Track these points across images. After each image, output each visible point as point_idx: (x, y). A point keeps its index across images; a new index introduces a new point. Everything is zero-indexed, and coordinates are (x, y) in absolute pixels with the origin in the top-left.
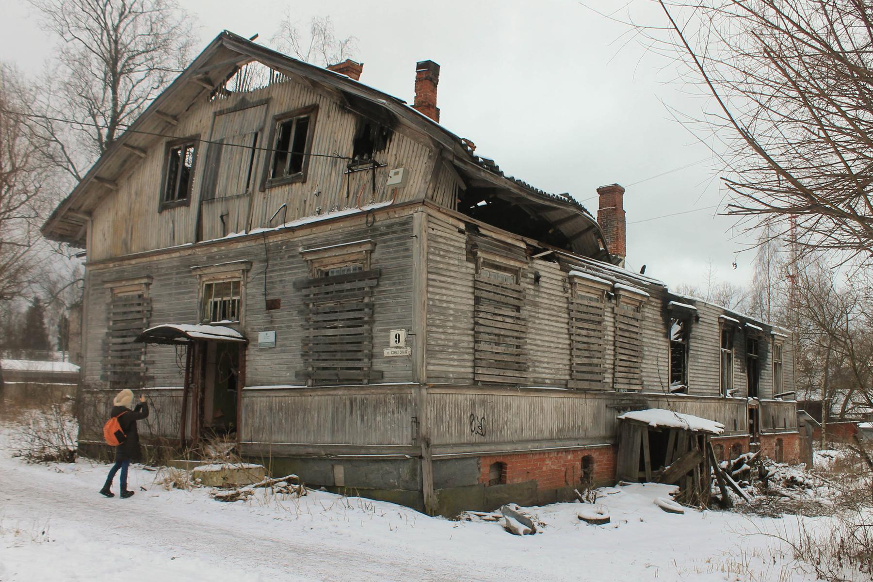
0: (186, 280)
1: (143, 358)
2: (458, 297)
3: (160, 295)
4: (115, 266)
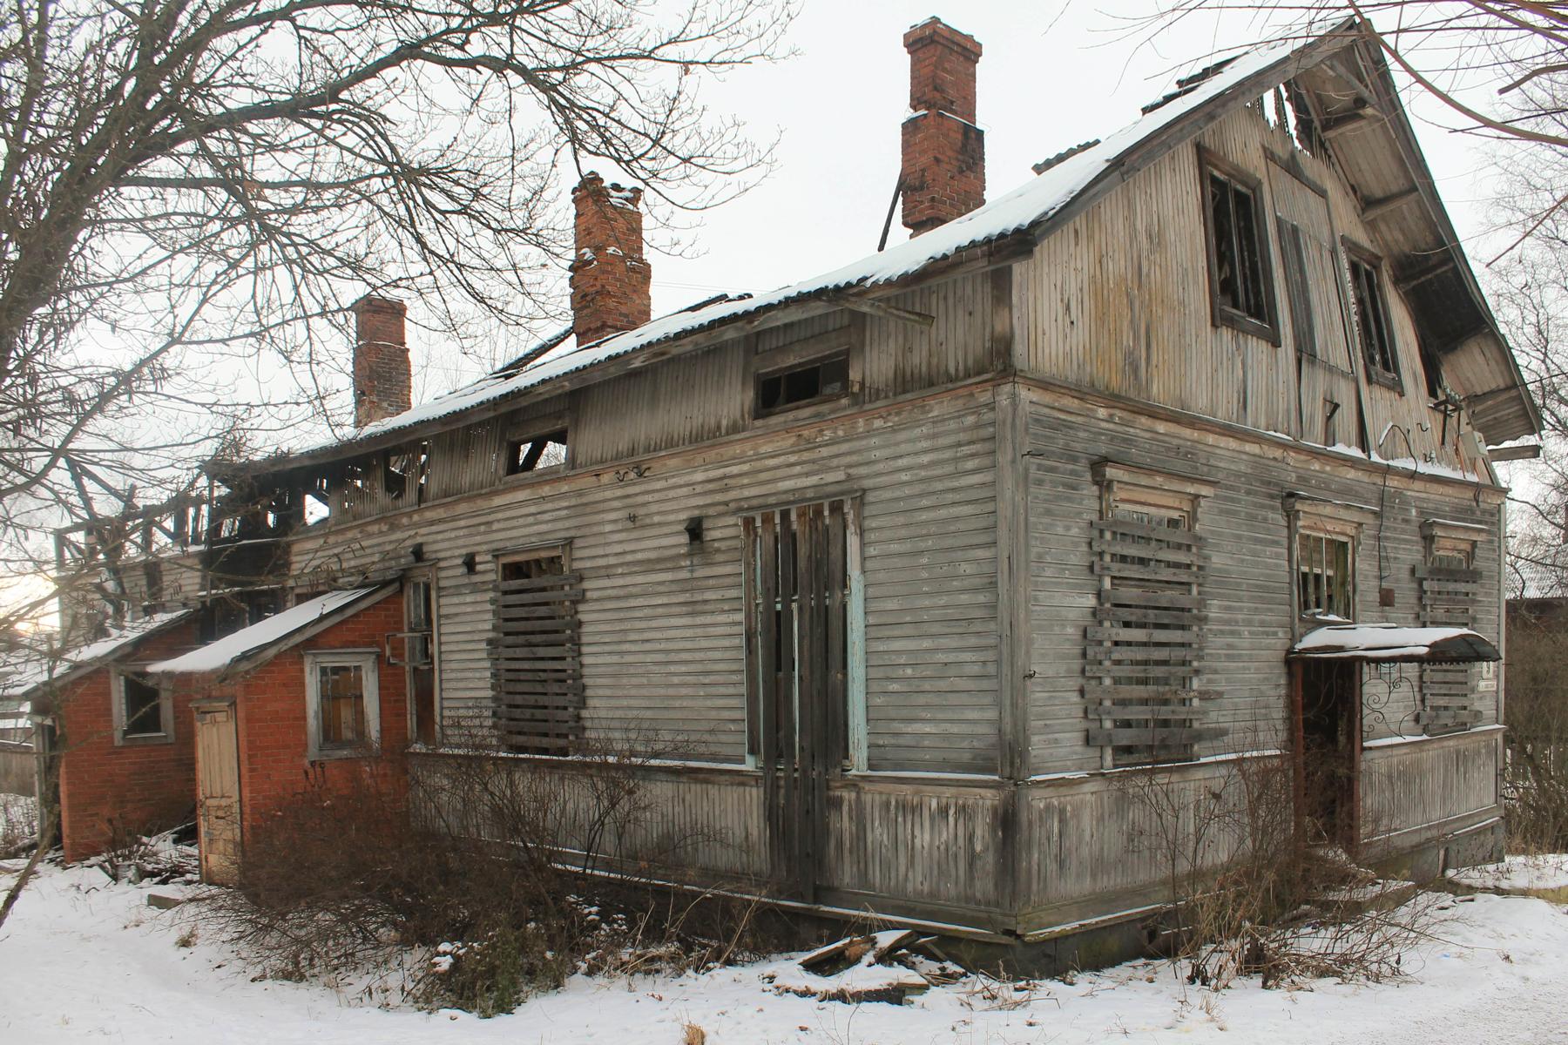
1: (1196, 684)
3: (1220, 534)
4: (1110, 419)
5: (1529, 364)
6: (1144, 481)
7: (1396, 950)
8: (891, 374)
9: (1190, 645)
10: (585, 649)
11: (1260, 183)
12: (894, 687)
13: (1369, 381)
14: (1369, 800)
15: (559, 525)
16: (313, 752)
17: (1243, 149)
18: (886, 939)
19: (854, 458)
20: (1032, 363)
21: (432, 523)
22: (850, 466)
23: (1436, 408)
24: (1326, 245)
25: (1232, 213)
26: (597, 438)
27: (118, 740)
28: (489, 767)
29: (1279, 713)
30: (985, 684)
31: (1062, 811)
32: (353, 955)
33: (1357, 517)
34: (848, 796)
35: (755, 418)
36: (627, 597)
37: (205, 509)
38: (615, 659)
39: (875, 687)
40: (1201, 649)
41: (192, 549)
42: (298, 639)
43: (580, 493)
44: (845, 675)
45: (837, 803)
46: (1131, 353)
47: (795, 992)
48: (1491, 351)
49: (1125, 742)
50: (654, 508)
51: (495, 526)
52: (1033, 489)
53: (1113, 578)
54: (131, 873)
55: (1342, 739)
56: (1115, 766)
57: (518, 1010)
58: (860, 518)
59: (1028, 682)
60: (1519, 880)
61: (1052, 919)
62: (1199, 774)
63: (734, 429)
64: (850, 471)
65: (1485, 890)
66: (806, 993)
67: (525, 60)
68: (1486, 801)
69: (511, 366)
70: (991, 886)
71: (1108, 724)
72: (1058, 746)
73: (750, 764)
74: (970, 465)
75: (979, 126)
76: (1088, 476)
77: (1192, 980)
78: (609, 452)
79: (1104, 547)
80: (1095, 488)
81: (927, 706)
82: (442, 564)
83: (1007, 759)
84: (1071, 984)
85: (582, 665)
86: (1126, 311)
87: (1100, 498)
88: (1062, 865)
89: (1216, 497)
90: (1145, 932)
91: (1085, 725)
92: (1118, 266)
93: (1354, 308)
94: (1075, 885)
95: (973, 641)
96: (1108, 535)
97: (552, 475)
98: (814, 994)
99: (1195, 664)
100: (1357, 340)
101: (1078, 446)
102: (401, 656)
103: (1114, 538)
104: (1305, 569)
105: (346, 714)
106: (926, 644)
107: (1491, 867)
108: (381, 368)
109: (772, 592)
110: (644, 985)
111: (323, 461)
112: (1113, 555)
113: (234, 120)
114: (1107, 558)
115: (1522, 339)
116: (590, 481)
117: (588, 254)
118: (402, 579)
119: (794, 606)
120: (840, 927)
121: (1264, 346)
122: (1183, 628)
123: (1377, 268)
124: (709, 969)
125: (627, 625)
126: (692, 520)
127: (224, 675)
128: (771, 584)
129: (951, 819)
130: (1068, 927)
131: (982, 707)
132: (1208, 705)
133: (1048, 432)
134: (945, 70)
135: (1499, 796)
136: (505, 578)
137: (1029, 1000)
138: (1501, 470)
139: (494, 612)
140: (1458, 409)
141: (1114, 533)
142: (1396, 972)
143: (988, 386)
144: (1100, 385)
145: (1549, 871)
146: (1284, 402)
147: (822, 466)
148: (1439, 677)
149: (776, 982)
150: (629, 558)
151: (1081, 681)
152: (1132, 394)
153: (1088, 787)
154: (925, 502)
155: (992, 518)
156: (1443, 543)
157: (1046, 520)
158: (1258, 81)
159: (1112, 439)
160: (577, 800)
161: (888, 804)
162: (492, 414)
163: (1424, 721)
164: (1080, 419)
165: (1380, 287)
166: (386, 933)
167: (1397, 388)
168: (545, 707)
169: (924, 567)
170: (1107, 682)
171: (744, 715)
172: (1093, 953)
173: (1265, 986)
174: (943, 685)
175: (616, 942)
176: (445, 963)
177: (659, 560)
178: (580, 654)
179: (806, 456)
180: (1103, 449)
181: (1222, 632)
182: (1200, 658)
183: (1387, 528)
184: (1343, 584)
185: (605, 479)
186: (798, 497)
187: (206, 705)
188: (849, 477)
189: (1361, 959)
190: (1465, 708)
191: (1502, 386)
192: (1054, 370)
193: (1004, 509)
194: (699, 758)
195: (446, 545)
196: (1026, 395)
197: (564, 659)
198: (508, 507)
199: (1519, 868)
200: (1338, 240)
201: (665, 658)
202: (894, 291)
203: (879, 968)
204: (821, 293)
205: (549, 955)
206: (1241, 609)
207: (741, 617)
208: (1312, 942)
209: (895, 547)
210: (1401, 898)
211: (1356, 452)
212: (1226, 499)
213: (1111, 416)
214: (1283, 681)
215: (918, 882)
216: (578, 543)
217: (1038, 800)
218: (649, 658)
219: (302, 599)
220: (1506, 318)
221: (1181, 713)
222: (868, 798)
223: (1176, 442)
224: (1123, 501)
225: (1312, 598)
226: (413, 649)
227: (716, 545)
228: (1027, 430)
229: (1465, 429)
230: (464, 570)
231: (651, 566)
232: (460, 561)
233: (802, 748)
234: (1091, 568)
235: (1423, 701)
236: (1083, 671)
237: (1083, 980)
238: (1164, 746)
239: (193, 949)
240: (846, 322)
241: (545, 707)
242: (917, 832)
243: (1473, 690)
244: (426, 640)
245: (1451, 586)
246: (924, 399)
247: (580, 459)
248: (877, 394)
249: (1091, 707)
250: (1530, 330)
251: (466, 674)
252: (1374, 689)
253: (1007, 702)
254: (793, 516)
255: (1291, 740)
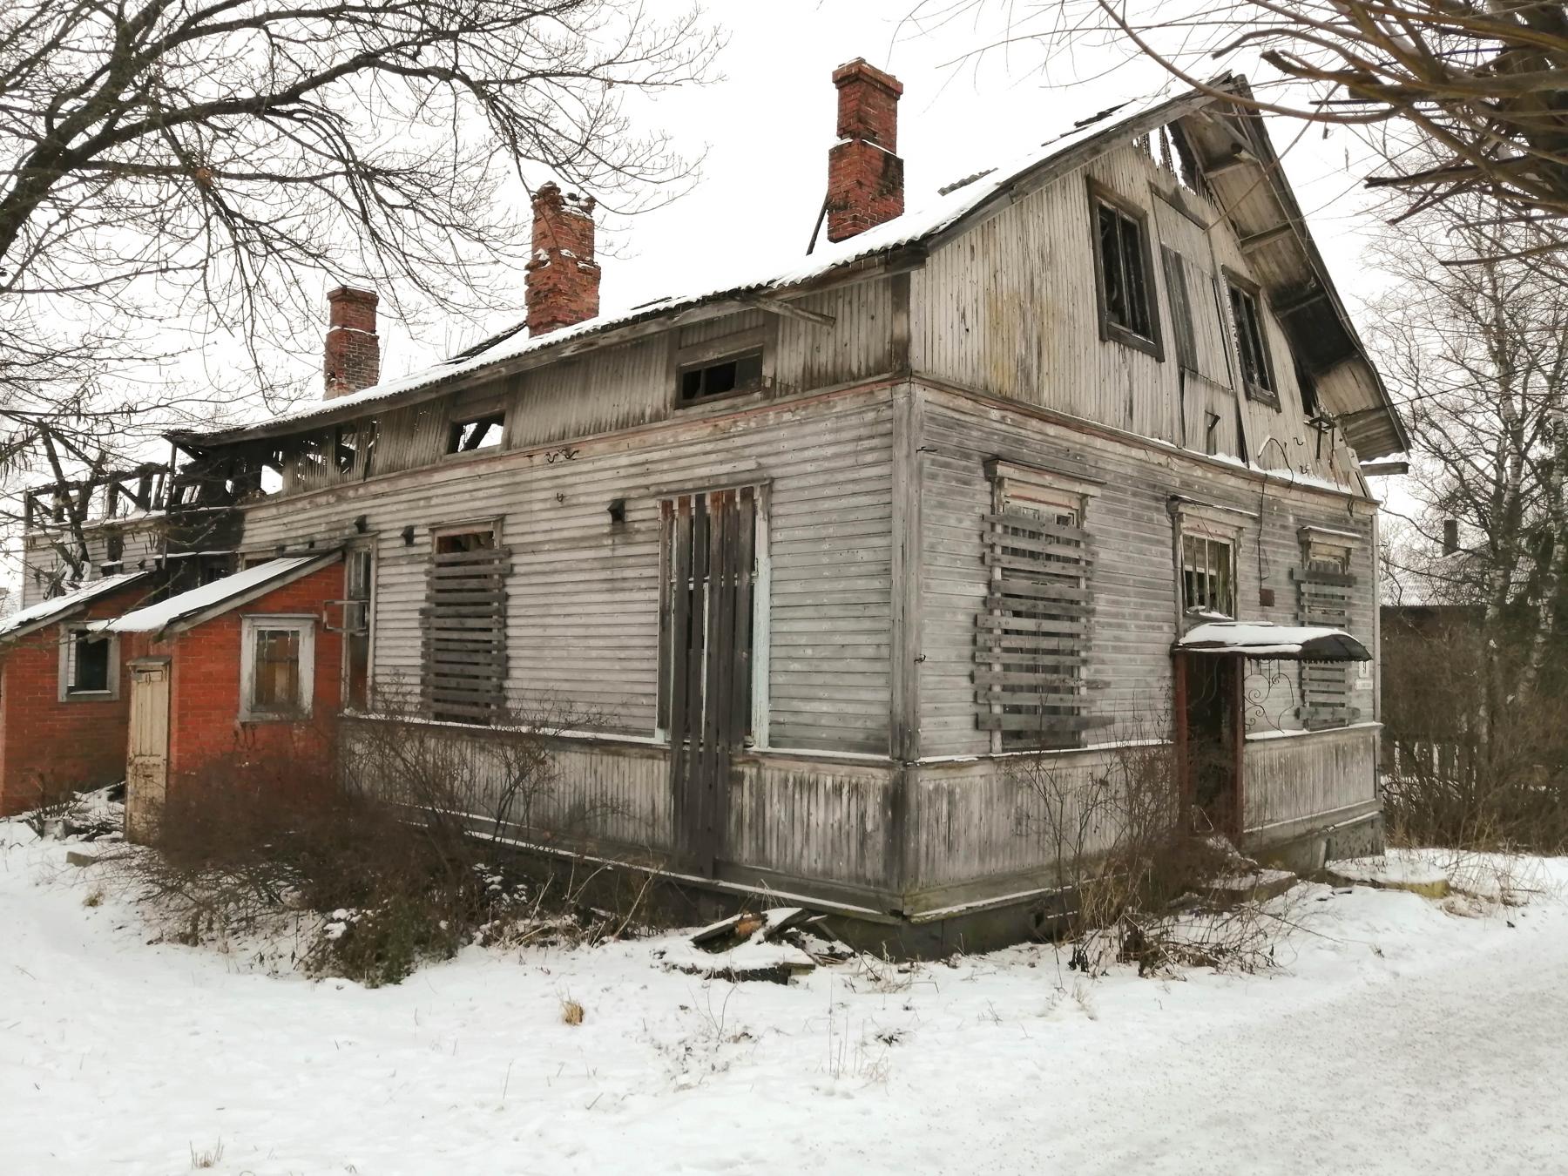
0: (1147, 513)
1: (1084, 673)
2: (596, 659)
3: (1108, 532)
4: (1003, 420)
5: (1400, 393)
6: (1034, 478)
7: (1270, 941)
8: (800, 370)
9: (1078, 636)
10: (510, 622)
11: (1145, 214)
12: (795, 666)
13: (1248, 397)
14: (1252, 792)
15: (493, 502)
16: (244, 715)
17: (1130, 182)
18: (776, 917)
19: (764, 449)
20: (929, 366)
21: (376, 496)
22: (761, 456)
23: (1311, 424)
24: (1208, 272)
25: (1118, 238)
26: (536, 420)
27: (62, 696)
28: (402, 733)
29: (1163, 705)
30: (878, 667)
31: (951, 793)
32: (253, 918)
33: (1237, 521)
34: (750, 771)
35: (677, 408)
36: (555, 572)
37: (167, 477)
38: (538, 632)
39: (777, 666)
40: (1089, 640)
41: (155, 514)
42: (238, 602)
43: (513, 472)
44: (750, 653)
45: (740, 778)
46: (1023, 361)
47: (682, 969)
48: (1361, 374)
49: (1014, 728)
50: (581, 489)
51: (434, 502)
52: (927, 483)
53: (1003, 569)
54: (58, 829)
55: (1226, 731)
56: (1004, 750)
57: (407, 981)
58: (769, 505)
59: (919, 665)
60: (1394, 875)
61: (939, 900)
62: (1088, 760)
63: (657, 417)
64: (763, 461)
65: (1363, 882)
66: (692, 971)
67: (468, 71)
68: (1365, 795)
69: (465, 354)
70: (880, 867)
71: (997, 709)
72: (948, 729)
73: (659, 738)
74: (869, 458)
75: (899, 155)
76: (981, 473)
77: (1072, 965)
78: (542, 436)
79: (995, 540)
80: (988, 484)
81: (824, 686)
82: (383, 536)
83: (898, 740)
84: (955, 967)
85: (507, 637)
86: (1018, 320)
87: (992, 493)
88: (950, 847)
89: (1104, 497)
90: (1032, 916)
91: (974, 709)
92: (1011, 280)
93: (1233, 331)
94: (963, 867)
95: (867, 624)
96: (999, 529)
97: (491, 456)
98: (700, 972)
99: (1083, 654)
100: (1237, 359)
101: (971, 444)
102: (339, 624)
103: (1005, 532)
104: (1189, 568)
105: (281, 679)
106: (826, 625)
107: (1368, 860)
108: (352, 351)
109: (686, 572)
110: (534, 954)
111: (276, 434)
112: (1005, 549)
113: (198, 114)
114: (998, 550)
115: (1395, 368)
116: (523, 462)
117: (544, 256)
118: (345, 549)
119: (706, 585)
120: (736, 902)
121: (1148, 360)
122: (1072, 619)
123: (1256, 296)
124: (603, 943)
125: (552, 600)
126: (615, 501)
127: (159, 635)
128: (686, 564)
129: (845, 798)
130: (955, 909)
131: (875, 688)
132: (1096, 694)
133: (941, 430)
134: (869, 105)
135: (1379, 789)
136: (439, 552)
137: (910, 984)
138: (1376, 486)
139: (428, 583)
140: (1332, 426)
141: (1006, 527)
142: (1270, 963)
143: (887, 385)
144: (994, 389)
145: (1423, 866)
146: (1169, 411)
147: (735, 455)
148: (1317, 674)
149: (666, 958)
150: (556, 536)
151: (970, 667)
152: (1024, 399)
153: (979, 770)
154: (828, 492)
155: (887, 510)
156: (1319, 549)
157: (940, 512)
158: (1141, 122)
159: (1004, 439)
160: (485, 770)
161: (787, 780)
162: (434, 396)
163: (1303, 716)
164: (973, 419)
165: (1259, 313)
166: (289, 895)
167: (1274, 404)
168: (477, 677)
169: (825, 553)
170: (997, 668)
171: (655, 689)
172: (981, 935)
173: (1141, 974)
174: (839, 666)
175: (519, 911)
176: (337, 930)
177: (583, 539)
178: (506, 626)
179: (722, 445)
180: (996, 448)
181: (1110, 625)
182: (1088, 649)
183: (1267, 533)
184: (1226, 583)
185: (537, 460)
186: (713, 484)
187: (142, 664)
188: (760, 467)
189: (1237, 950)
190: (1343, 705)
191: (1372, 406)
192: (950, 373)
193: (899, 501)
194: (613, 729)
195: (388, 517)
196: (922, 395)
197: (490, 630)
198: (446, 483)
199: (1395, 862)
200: (1219, 269)
201: (585, 636)
202: (801, 294)
203: (768, 946)
204: (734, 294)
205: (443, 924)
206: (1128, 603)
207: (656, 595)
208: (1191, 929)
209: (799, 534)
210: (1280, 888)
211: (1236, 462)
212: (1114, 499)
213: (1004, 418)
214: (1168, 674)
215: (812, 860)
216: (509, 520)
217: (926, 781)
218: (570, 632)
219: (251, 564)
220: (1377, 348)
221: (1068, 701)
222: (767, 774)
223: (1065, 444)
224: (1014, 497)
225: (1196, 595)
226: (351, 616)
227: (637, 526)
228: (922, 428)
229: (1339, 445)
230: (403, 542)
231: (575, 544)
232: (399, 534)
233: (707, 723)
234: (982, 559)
235: (1302, 696)
236: (973, 657)
237: (966, 963)
238: (1053, 732)
239: (99, 909)
240: (761, 322)
241: (477, 677)
242: (813, 810)
243: (1350, 688)
244: (364, 608)
245: (1328, 590)
246: (828, 394)
247: (516, 440)
248: (787, 389)
249: (981, 692)
250: (1403, 360)
251: (398, 644)
252: (1255, 684)
253: (899, 685)
254: (708, 502)
255: (1175, 734)
